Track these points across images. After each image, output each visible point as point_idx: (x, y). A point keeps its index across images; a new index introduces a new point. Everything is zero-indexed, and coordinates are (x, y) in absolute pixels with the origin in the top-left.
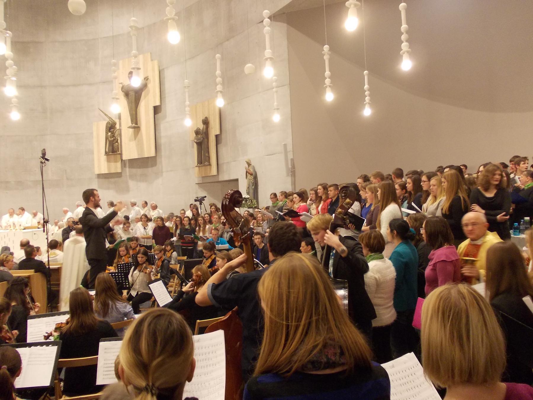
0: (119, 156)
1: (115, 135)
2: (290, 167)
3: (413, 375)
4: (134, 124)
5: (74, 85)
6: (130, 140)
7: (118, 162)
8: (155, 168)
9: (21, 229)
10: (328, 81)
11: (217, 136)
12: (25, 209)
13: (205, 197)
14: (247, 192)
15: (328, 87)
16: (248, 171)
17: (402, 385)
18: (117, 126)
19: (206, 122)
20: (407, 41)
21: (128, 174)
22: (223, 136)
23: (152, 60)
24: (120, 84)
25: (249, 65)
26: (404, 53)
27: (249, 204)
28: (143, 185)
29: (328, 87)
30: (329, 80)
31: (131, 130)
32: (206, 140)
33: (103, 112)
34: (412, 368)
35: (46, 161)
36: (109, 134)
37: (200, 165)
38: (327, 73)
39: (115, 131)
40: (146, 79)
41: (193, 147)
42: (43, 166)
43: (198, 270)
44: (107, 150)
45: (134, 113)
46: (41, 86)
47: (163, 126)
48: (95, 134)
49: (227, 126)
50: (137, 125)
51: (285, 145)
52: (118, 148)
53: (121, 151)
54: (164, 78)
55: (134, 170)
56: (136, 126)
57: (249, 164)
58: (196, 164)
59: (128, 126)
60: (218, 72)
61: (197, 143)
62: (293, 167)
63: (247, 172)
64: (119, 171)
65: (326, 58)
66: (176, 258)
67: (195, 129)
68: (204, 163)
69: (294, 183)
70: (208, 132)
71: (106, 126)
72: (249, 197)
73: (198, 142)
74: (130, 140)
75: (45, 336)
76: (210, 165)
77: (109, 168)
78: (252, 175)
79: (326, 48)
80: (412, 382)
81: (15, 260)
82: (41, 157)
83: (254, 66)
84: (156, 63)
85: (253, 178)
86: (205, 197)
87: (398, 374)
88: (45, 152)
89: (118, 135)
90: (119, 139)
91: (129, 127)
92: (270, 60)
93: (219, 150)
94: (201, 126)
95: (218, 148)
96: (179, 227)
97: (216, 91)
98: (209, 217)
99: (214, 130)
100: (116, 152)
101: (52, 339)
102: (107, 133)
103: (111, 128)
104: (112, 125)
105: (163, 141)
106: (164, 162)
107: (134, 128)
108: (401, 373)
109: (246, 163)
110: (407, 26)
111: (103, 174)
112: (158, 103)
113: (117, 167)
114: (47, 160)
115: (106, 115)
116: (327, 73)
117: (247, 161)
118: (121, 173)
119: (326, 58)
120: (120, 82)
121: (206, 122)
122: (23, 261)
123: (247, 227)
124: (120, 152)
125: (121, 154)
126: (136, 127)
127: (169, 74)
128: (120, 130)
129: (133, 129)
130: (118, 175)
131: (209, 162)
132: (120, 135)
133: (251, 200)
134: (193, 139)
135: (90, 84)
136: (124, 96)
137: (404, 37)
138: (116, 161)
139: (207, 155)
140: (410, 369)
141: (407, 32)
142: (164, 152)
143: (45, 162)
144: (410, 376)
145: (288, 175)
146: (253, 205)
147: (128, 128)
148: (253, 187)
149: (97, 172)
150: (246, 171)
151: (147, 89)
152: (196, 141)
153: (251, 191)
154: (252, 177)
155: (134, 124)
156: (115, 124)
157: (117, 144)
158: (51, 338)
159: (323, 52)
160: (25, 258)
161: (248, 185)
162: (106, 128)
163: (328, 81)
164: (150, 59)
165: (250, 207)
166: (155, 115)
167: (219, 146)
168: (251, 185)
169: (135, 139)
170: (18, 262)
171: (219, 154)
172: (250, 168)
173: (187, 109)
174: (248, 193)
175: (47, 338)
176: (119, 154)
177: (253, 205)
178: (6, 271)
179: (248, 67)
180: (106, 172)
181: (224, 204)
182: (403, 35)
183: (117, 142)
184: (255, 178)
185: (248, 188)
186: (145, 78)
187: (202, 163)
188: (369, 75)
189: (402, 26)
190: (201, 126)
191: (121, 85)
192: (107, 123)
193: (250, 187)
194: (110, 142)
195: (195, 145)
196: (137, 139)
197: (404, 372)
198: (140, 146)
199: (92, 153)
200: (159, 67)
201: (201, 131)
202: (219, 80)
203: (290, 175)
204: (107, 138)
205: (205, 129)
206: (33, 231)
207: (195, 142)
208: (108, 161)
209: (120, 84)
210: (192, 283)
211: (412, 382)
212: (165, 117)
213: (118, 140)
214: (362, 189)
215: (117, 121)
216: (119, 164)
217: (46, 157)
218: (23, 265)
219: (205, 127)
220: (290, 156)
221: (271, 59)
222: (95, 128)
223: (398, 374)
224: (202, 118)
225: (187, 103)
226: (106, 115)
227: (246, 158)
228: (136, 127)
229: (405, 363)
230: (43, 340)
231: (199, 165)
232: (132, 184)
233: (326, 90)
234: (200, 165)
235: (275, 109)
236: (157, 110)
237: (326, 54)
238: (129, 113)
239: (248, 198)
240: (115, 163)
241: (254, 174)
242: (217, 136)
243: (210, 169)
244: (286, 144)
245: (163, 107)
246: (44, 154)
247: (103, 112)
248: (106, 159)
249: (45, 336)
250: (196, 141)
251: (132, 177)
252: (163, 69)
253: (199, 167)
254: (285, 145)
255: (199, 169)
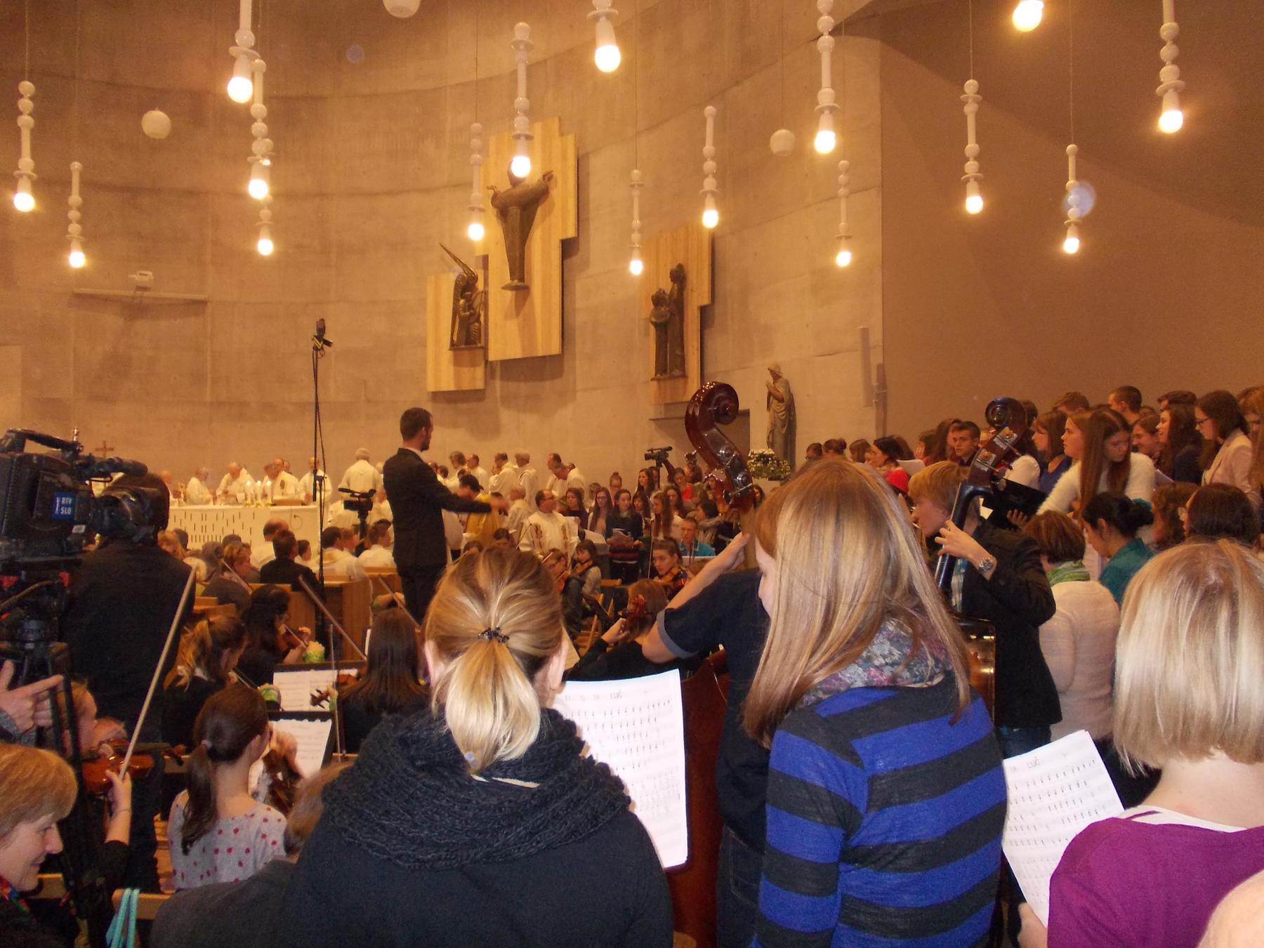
0: (481, 352)
1: (475, 306)
2: (874, 383)
3: (1082, 785)
4: (516, 281)
5: (390, 193)
6: (506, 317)
7: (478, 365)
8: (558, 382)
9: (268, 504)
10: (971, 167)
11: (703, 310)
12: (321, 317)
13: (670, 448)
14: (768, 443)
15: (972, 180)
16: (773, 391)
17: (1066, 820)
18: (480, 285)
19: (679, 276)
20: (1174, 62)
21: (498, 394)
22: (718, 309)
23: (562, 134)
24: (488, 188)
25: (782, 132)
26: (1166, 91)
27: (772, 469)
28: (530, 420)
29: (972, 180)
30: (976, 163)
31: (509, 294)
32: (677, 318)
33: (449, 253)
34: (1081, 768)
35: (325, 346)
36: (462, 302)
37: (662, 377)
38: (972, 147)
39: (474, 296)
40: (546, 178)
41: (647, 334)
42: (319, 356)
43: (640, 590)
44: (455, 339)
45: (518, 255)
46: (322, 195)
47: (580, 285)
48: (430, 300)
49: (729, 285)
50: (524, 281)
51: (865, 333)
52: (480, 335)
53: (487, 342)
54: (588, 174)
55: (512, 386)
56: (519, 284)
57: (776, 376)
58: (653, 374)
59: (503, 285)
60: (709, 148)
61: (656, 325)
62: (883, 383)
63: (770, 394)
64: (480, 385)
65: (970, 110)
66: (597, 582)
67: (654, 292)
68: (671, 372)
69: (882, 422)
70: (682, 299)
71: (456, 285)
72: (771, 452)
73: (658, 321)
74: (506, 317)
75: (313, 697)
76: (684, 376)
77: (457, 377)
78: (781, 400)
79: (971, 85)
80: (1078, 803)
81: (253, 563)
82: (316, 337)
83: (792, 136)
84: (570, 140)
85: (783, 408)
86: (670, 448)
87: (1046, 781)
88: (324, 327)
89: (480, 304)
90: (482, 313)
91: (505, 288)
92: (831, 113)
93: (710, 345)
94: (667, 285)
95: (706, 337)
96: (604, 512)
97: (701, 191)
98: (677, 497)
99: (698, 295)
100: (476, 343)
101: (326, 706)
102: (456, 301)
103: (466, 288)
104: (468, 282)
105: (580, 319)
106: (580, 368)
107: (516, 288)
108: (1054, 778)
109: (769, 372)
110: (1174, 24)
111: (443, 392)
112: (571, 233)
113: (475, 378)
114: (328, 343)
115: (456, 259)
116: (972, 147)
117: (772, 368)
118: (482, 392)
119: (970, 110)
120: (490, 185)
121: (679, 276)
122: (271, 563)
123: (727, 442)
124: (483, 343)
125: (485, 349)
126: (521, 286)
127: (598, 165)
128: (486, 293)
129: (514, 292)
130: (475, 396)
131: (684, 370)
132: (485, 305)
133: (778, 462)
134: (648, 316)
135: (426, 191)
136: (497, 217)
137: (1167, 52)
138: (473, 364)
139: (678, 352)
140: (1076, 770)
141: (1176, 41)
142: (581, 346)
143: (322, 348)
144: (1075, 788)
145: (868, 404)
146: (782, 472)
147: (503, 288)
148: (784, 431)
149: (431, 388)
150: (767, 391)
151: (547, 203)
152: (653, 320)
153: (779, 440)
154: (782, 407)
155: (516, 281)
156: (475, 279)
157: (477, 324)
158: (324, 703)
159: (962, 97)
160: (274, 558)
161: (772, 423)
162: (456, 289)
163: (971, 167)
164: (557, 133)
165: (773, 475)
166: (565, 262)
167: (707, 332)
168: (779, 425)
169: (518, 314)
170: (259, 567)
171: (708, 352)
172: (777, 385)
173: (636, 237)
174: (771, 445)
175: (316, 701)
176: (481, 347)
177: (782, 472)
178: (236, 581)
179: (781, 139)
180: (452, 388)
181: (691, 412)
182: (1164, 48)
183: (478, 320)
184: (790, 408)
185: (772, 432)
186: (544, 176)
187: (665, 372)
188: (1078, 156)
189: (1162, 24)
190: (667, 285)
191: (491, 192)
192: (458, 277)
193: (776, 430)
194: (462, 319)
195: (652, 329)
196: (521, 314)
197: (1061, 776)
198: (528, 329)
199: (423, 343)
200: (578, 149)
201: (667, 297)
202: (709, 165)
203: (874, 404)
204: (455, 312)
205: (675, 293)
206: (291, 510)
207: (652, 323)
208: (457, 362)
209: (488, 188)
210: (622, 623)
211: (1078, 803)
212: (586, 264)
213: (479, 315)
214: (1040, 428)
215: (480, 274)
216: (480, 371)
217: (326, 337)
218: (270, 572)
219: (676, 288)
220: (876, 358)
221: (832, 109)
222: (430, 289)
223: (1046, 781)
224: (671, 266)
225: (637, 222)
226: (456, 259)
227: (770, 362)
228: (521, 286)
229: (1065, 755)
230: (307, 707)
231: (658, 375)
232: (506, 416)
233: (966, 188)
234: (662, 377)
235: (840, 238)
236: (568, 248)
237: (970, 100)
238: (506, 255)
239: (771, 456)
240: (472, 369)
241: (786, 398)
242: (703, 310)
243: (686, 383)
244: (868, 329)
245: (582, 240)
246: (321, 331)
247: (449, 253)
248: (452, 358)
249: (313, 697)
250: (653, 320)
251: (508, 400)
252: (587, 154)
253: (659, 380)
254: (865, 333)
255: (659, 386)
